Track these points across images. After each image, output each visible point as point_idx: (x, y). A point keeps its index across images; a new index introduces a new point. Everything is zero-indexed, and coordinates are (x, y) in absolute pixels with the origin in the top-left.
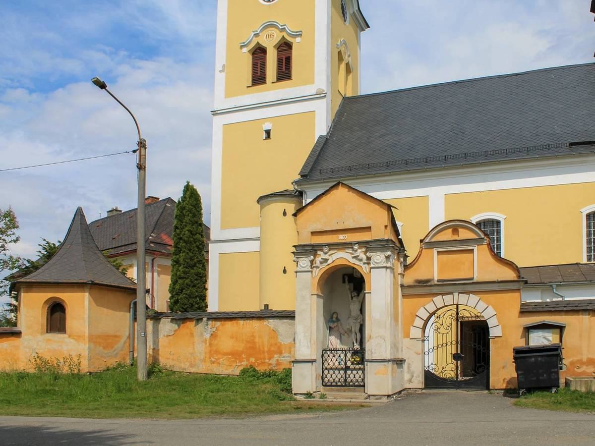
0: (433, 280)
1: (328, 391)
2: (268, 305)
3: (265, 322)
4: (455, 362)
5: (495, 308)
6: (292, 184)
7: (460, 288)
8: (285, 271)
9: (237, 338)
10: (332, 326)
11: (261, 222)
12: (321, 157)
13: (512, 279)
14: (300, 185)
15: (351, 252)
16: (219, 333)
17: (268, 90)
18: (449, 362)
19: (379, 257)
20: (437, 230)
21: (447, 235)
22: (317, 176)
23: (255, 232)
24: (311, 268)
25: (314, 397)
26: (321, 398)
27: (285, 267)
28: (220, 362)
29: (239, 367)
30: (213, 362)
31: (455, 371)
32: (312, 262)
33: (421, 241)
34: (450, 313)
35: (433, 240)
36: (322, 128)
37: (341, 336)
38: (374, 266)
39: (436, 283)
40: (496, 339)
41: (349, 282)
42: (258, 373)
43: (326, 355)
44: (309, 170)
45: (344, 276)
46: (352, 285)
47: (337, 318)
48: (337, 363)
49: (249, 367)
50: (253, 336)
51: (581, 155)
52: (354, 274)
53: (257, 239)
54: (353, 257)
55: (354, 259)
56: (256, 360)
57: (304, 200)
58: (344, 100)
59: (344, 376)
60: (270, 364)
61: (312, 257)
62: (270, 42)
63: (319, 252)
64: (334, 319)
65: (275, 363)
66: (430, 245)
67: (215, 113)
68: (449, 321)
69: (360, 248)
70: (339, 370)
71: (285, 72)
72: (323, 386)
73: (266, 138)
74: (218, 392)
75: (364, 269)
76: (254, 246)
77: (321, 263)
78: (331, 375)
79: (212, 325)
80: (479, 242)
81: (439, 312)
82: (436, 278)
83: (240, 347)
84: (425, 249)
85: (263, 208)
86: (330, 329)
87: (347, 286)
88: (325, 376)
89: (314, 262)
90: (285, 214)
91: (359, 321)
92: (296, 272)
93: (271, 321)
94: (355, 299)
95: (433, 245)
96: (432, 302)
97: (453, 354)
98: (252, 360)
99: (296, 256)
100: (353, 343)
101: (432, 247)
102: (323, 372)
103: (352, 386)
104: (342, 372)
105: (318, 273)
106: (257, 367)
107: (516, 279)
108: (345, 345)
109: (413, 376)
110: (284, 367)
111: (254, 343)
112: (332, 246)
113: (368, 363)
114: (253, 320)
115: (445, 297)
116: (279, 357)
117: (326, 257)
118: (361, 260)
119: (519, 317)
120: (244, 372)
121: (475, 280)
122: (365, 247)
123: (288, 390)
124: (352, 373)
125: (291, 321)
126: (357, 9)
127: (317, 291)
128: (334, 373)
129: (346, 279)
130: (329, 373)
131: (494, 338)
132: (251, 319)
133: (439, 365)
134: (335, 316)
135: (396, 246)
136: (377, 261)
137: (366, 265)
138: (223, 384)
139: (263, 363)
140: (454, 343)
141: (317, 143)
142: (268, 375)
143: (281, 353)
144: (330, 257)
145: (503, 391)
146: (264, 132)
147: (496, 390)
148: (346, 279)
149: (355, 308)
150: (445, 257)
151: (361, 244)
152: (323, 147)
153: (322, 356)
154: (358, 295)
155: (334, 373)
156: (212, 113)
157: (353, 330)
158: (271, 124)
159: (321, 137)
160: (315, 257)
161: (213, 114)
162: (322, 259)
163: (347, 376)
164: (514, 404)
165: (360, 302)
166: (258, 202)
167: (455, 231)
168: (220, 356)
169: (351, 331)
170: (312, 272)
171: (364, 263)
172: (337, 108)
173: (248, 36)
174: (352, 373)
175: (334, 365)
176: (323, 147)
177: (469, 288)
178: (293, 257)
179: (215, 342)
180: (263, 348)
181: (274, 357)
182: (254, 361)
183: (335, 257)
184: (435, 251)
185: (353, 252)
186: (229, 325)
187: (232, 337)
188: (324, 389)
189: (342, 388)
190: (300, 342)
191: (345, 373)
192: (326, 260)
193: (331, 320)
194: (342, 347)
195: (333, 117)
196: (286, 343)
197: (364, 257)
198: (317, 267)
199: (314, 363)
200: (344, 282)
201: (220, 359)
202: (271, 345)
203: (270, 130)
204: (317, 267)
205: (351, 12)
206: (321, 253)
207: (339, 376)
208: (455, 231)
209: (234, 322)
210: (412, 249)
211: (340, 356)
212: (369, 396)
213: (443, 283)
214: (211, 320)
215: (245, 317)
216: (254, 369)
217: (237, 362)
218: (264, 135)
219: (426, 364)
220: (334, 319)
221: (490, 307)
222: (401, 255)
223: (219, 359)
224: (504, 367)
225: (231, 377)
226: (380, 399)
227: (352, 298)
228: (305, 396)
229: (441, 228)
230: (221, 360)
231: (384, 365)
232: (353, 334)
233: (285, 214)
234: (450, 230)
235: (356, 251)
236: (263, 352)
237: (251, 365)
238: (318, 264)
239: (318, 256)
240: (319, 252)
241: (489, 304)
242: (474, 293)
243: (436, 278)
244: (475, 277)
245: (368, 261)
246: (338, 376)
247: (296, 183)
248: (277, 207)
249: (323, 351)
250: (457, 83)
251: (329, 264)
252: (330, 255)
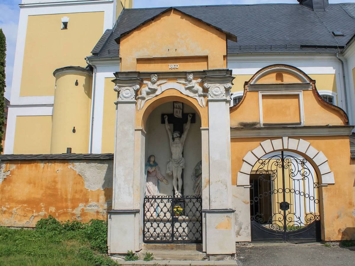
0: (259, 123)
1: (152, 248)
2: (71, 149)
3: (70, 166)
4: (282, 212)
5: (326, 154)
6: (85, 59)
7: (290, 132)
8: (74, 131)
9: (35, 184)
10: (151, 171)
11: (55, 89)
12: (108, 43)
13: (339, 125)
14: (92, 61)
15: (184, 82)
16: (14, 177)
20: (262, 73)
22: (106, 54)
23: (50, 100)
24: (136, 99)
25: (137, 258)
26: (145, 259)
27: (74, 127)
28: (13, 212)
29: (36, 218)
30: (4, 212)
31: (283, 222)
32: (137, 92)
35: (258, 83)
37: (158, 183)
38: (212, 98)
39: (262, 126)
40: (329, 187)
41: (169, 122)
42: (60, 225)
43: (148, 204)
44: (99, 50)
45: (163, 115)
46: (172, 125)
47: (154, 162)
48: (162, 214)
49: (48, 218)
50: (55, 182)
51: (305, 54)
52: (175, 114)
53: (52, 105)
54: (187, 89)
55: (188, 91)
56: (57, 209)
57: (94, 73)
58: (124, 11)
59: (171, 230)
60: (73, 215)
61: (138, 86)
63: (145, 82)
64: (152, 163)
65: (80, 213)
66: (255, 88)
67: (22, 6)
69: (194, 78)
70: (165, 222)
72: (145, 242)
73: (63, 28)
74: (9, 255)
75: (199, 102)
76: (48, 111)
77: (148, 94)
78: (155, 229)
79: (6, 168)
80: (305, 88)
82: (262, 122)
83: (38, 194)
84: (250, 91)
85: (58, 79)
86: (148, 173)
87: (168, 127)
88: (146, 230)
89: (139, 93)
90: (77, 84)
91: (181, 165)
92: (117, 104)
93: (77, 164)
94: (177, 140)
95: (258, 88)
96: (260, 146)
97: (280, 204)
98: (52, 209)
99: (118, 85)
100: (174, 191)
101: (257, 90)
102: (144, 225)
103: (181, 242)
104: (168, 225)
105: (143, 105)
106: (57, 217)
107: (343, 125)
108: (164, 193)
109: (241, 228)
110: (90, 219)
111: (56, 189)
112: (162, 75)
113: (207, 214)
114: (55, 162)
115: (274, 142)
116: (85, 206)
117: (154, 86)
118: (196, 92)
119: (350, 164)
120: (42, 224)
121: (302, 125)
122: (201, 78)
123: (101, 249)
124: (181, 226)
125: (99, 164)
127: (142, 126)
128: (158, 226)
129: (166, 120)
130: (152, 226)
131: (327, 186)
132: (53, 162)
134: (152, 159)
136: (216, 94)
137: (202, 98)
138: (16, 240)
139: (65, 213)
140: (287, 191)
141: (105, 33)
142: (73, 227)
143: (87, 201)
144: (159, 88)
145: (338, 244)
146: (62, 24)
147: (332, 242)
148: (166, 120)
150: (270, 101)
151: (196, 74)
153: (144, 205)
154: (180, 137)
155: (158, 226)
156: (20, 6)
157: (175, 175)
158: (69, 18)
159: (108, 30)
160: (140, 87)
161: (20, 7)
162: (149, 89)
163: (175, 230)
165: (182, 144)
166: (54, 74)
167: (279, 76)
168: (13, 205)
169: (172, 177)
170: (136, 103)
171: (200, 96)
172: (119, 14)
174: (181, 226)
175: (152, 216)
176: (110, 37)
177: (299, 132)
178: (114, 86)
179: (7, 188)
180: (66, 196)
181: (78, 206)
182: (54, 211)
183: (164, 87)
184: (260, 94)
185: (187, 83)
186: (26, 168)
187: (30, 183)
188: (147, 247)
189: (169, 244)
190: (119, 188)
191: (173, 226)
192: (154, 91)
193: (148, 163)
194: (162, 195)
195: (117, 19)
196: (93, 190)
197: (200, 89)
198: (143, 98)
199: (137, 214)
200: (163, 122)
201: (13, 208)
202: (76, 192)
203: (67, 22)
204: (143, 98)
206: (149, 83)
207: (165, 230)
208: (279, 76)
209: (33, 165)
211: (165, 206)
212: (208, 256)
213: (269, 127)
214: (6, 162)
215: (47, 159)
216: (55, 220)
217: (33, 212)
218: (62, 26)
220: (152, 163)
221: (321, 153)
223: (11, 208)
224: (338, 217)
225: (25, 231)
226: (222, 259)
227: (173, 139)
228: (124, 257)
229: (265, 71)
230: (14, 209)
231: (227, 216)
232: (175, 180)
233: (77, 84)
234: (275, 75)
235: (190, 81)
236: (66, 200)
237: (50, 215)
238: (144, 94)
239: (143, 85)
240: (145, 82)
241: (317, 148)
242: (305, 138)
243: (262, 122)
244: (302, 121)
245: (205, 93)
246: (165, 229)
247: (89, 59)
248: (70, 78)
249: (145, 199)
250: (207, 6)
251: (157, 96)
252: (158, 85)
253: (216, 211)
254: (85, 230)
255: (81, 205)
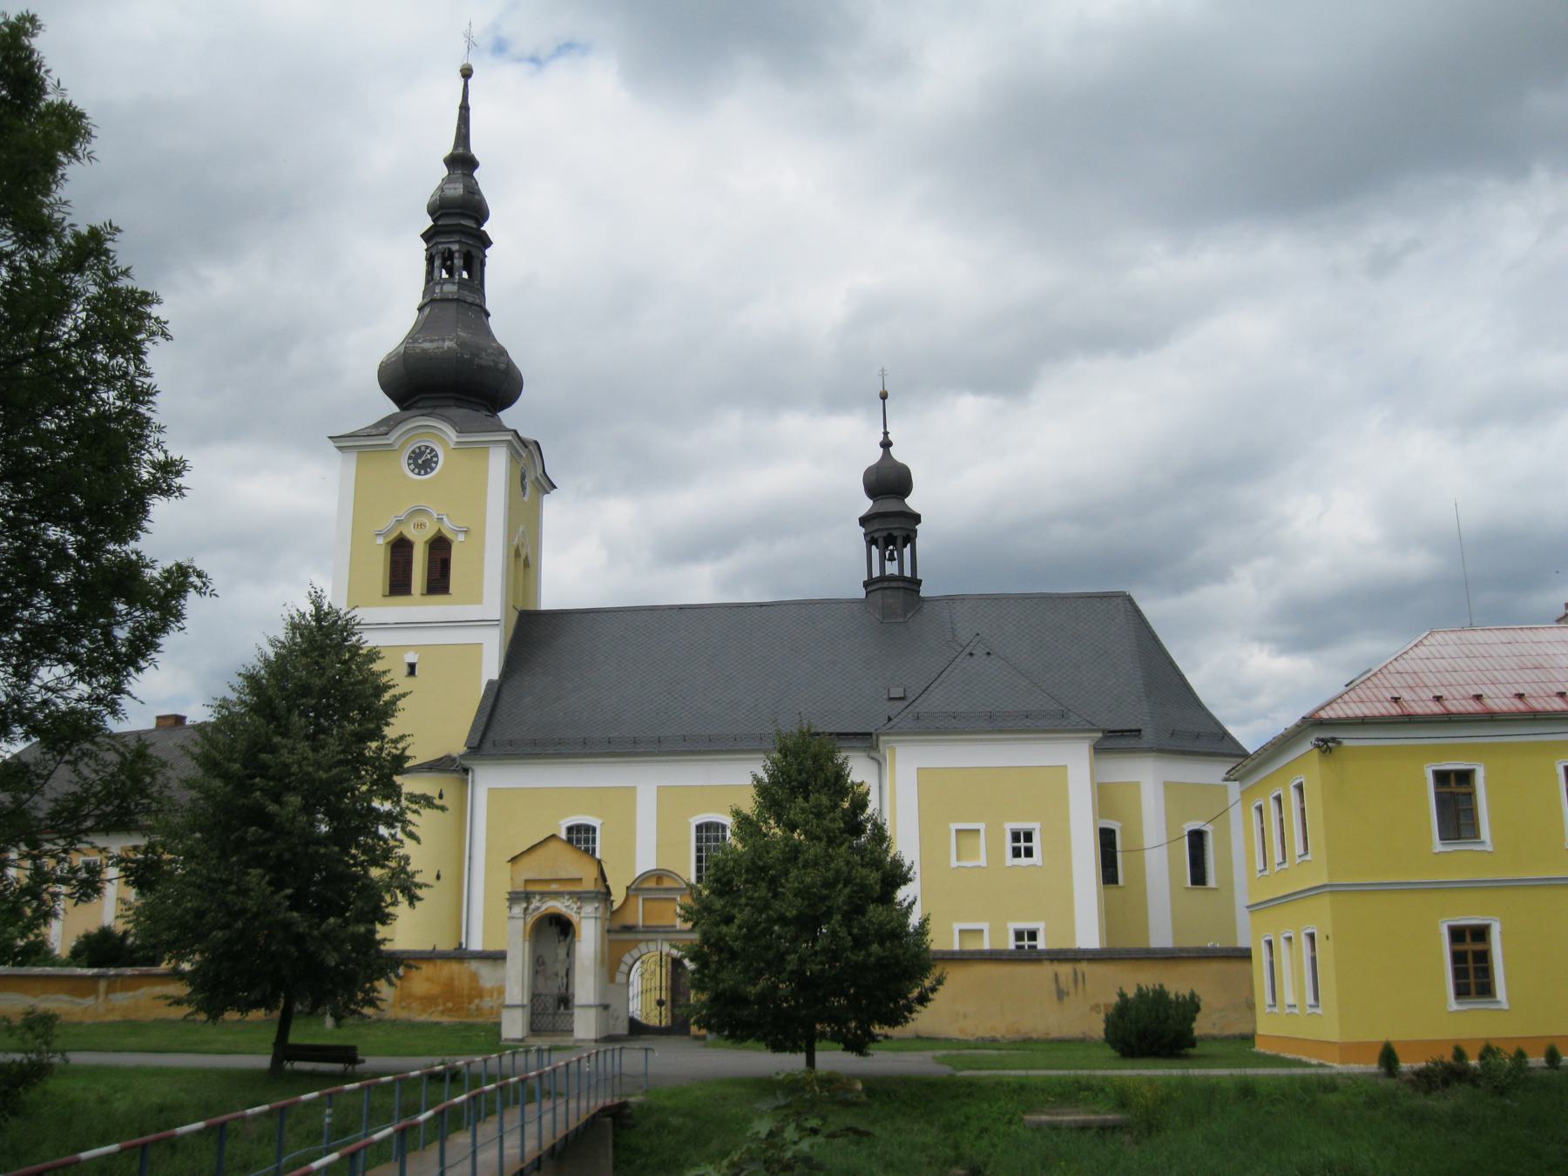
4: (659, 1008)
17: (414, 604)
18: (653, 1007)
19: (589, 909)
21: (652, 884)
33: (628, 888)
34: (654, 959)
36: (491, 668)
62: (420, 540)
64: (540, 962)
68: (653, 967)
71: (439, 582)
75: (575, 918)
81: (644, 958)
87: (555, 930)
104: (551, 1018)
105: (530, 920)
112: (543, 895)
126: (541, 471)
133: (644, 1010)
134: (541, 959)
135: (606, 895)
140: (658, 988)
143: (481, 997)
149: (562, 952)
151: (571, 894)
152: (496, 695)
159: (490, 683)
164: (186, 781)
169: (557, 975)
173: (386, 523)
200: (551, 924)
205: (533, 478)
210: (618, 897)
219: (631, 1010)
222: (608, 902)
232: (560, 978)
243: (641, 923)
253: (1314, 892)
254: (324, 1140)
255: (476, 1001)
